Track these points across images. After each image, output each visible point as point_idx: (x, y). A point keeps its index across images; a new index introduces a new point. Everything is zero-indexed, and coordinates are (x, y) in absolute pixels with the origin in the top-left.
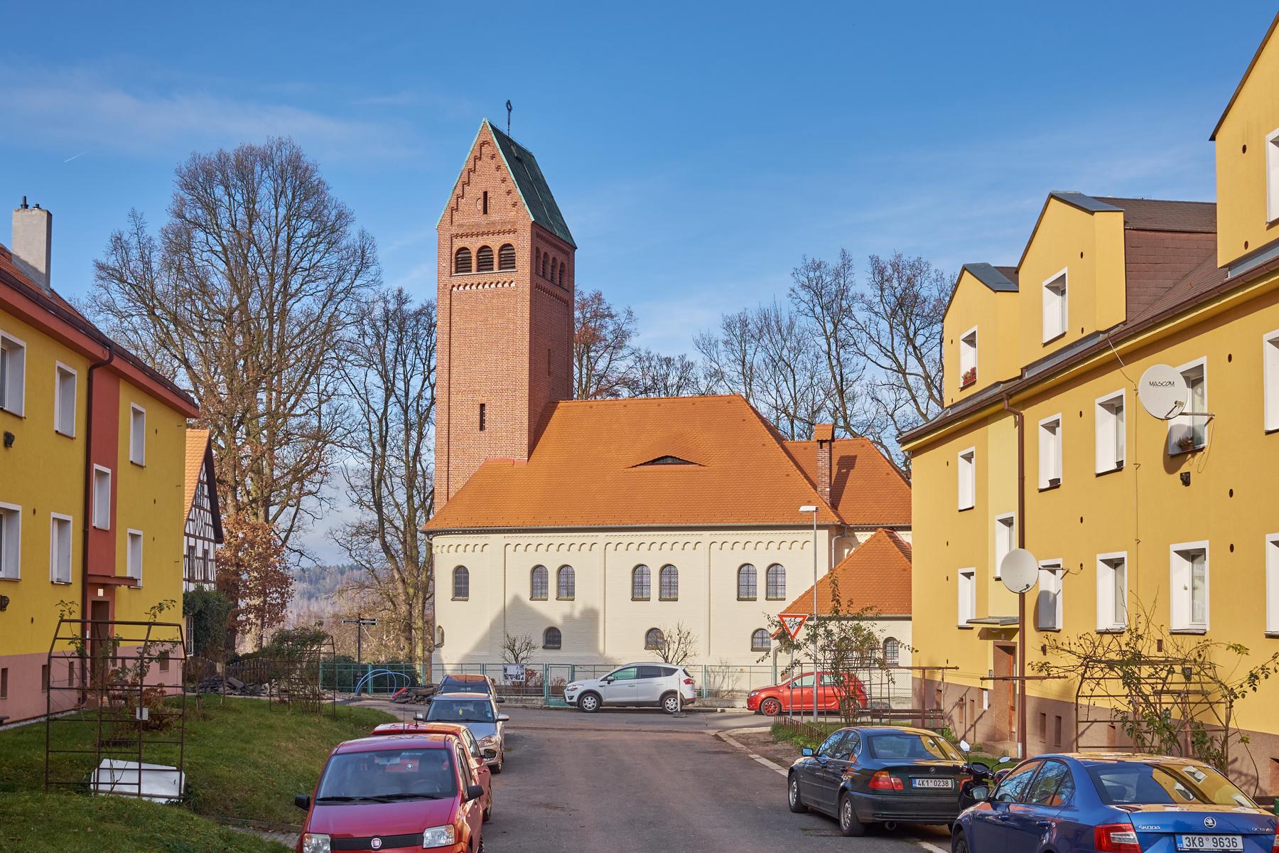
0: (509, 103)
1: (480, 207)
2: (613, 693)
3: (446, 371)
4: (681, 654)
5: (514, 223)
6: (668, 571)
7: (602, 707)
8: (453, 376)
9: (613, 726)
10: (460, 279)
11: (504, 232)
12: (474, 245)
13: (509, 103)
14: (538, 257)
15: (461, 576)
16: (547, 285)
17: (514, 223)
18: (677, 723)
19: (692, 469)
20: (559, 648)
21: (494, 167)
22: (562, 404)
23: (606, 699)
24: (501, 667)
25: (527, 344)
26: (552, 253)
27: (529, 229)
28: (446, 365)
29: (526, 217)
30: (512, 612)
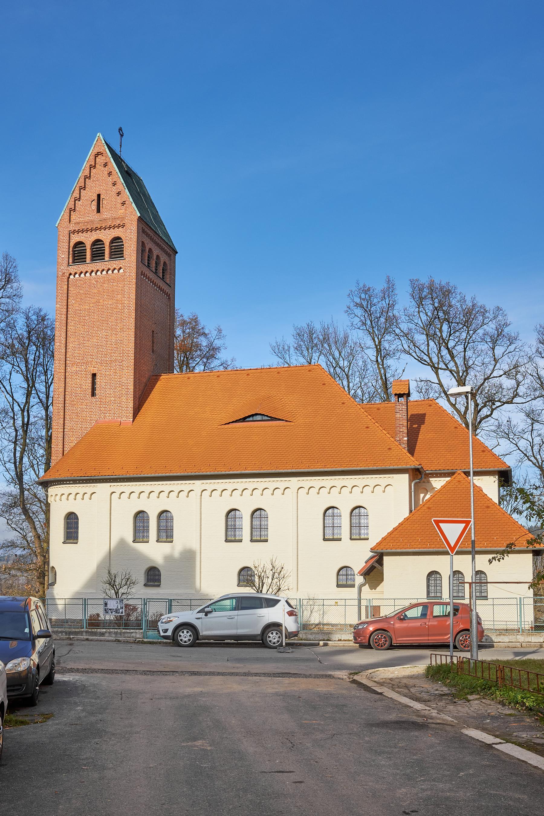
0: (120, 129)
1: (94, 207)
2: (209, 627)
3: (63, 346)
4: (275, 588)
5: (123, 218)
7: (199, 641)
8: (69, 350)
9: (212, 666)
10: (74, 268)
11: (114, 227)
12: (88, 239)
13: (120, 129)
14: (143, 251)
15: (72, 521)
16: (152, 275)
17: (123, 218)
18: (284, 660)
19: (271, 437)
20: (159, 586)
21: (106, 173)
22: (164, 377)
23: (203, 632)
24: (102, 602)
25: (133, 321)
26: (156, 251)
27: (135, 223)
28: (64, 341)
29: (133, 213)
30: (117, 554)
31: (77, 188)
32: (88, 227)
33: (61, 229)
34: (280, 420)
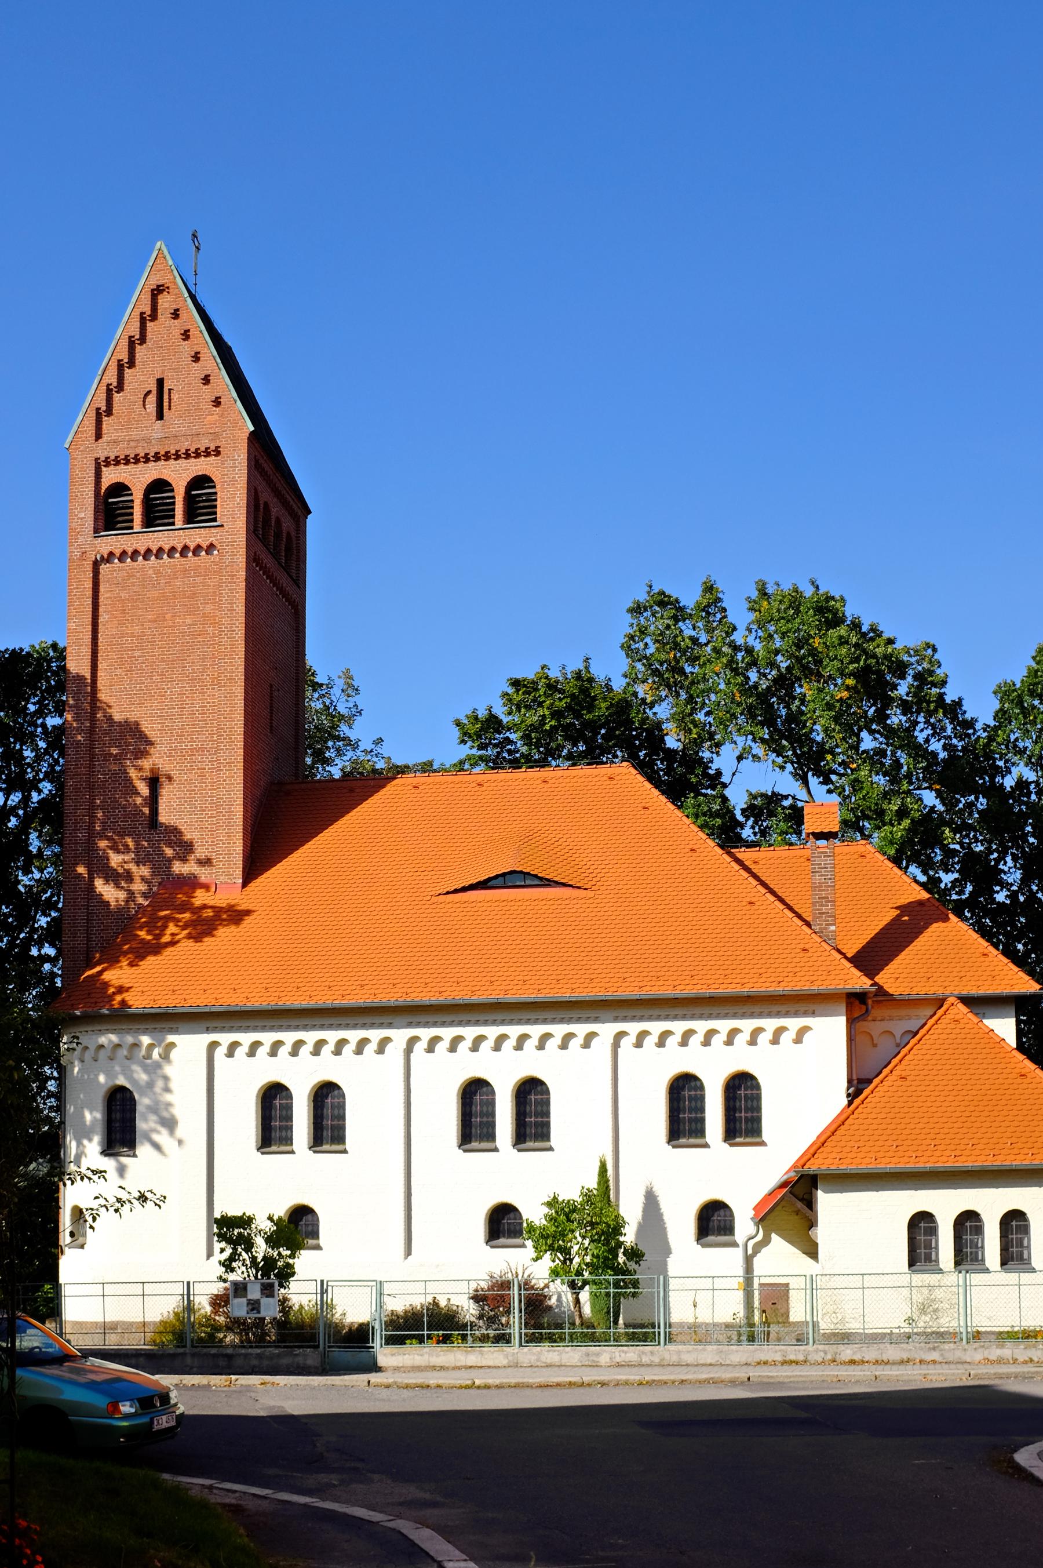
6: (326, 1096)
10: (113, 542)
11: (197, 454)
12: (138, 479)
24: (179, 1289)
26: (276, 510)
31: (113, 365)
32: (138, 452)
33: (77, 454)
34: (564, 885)
